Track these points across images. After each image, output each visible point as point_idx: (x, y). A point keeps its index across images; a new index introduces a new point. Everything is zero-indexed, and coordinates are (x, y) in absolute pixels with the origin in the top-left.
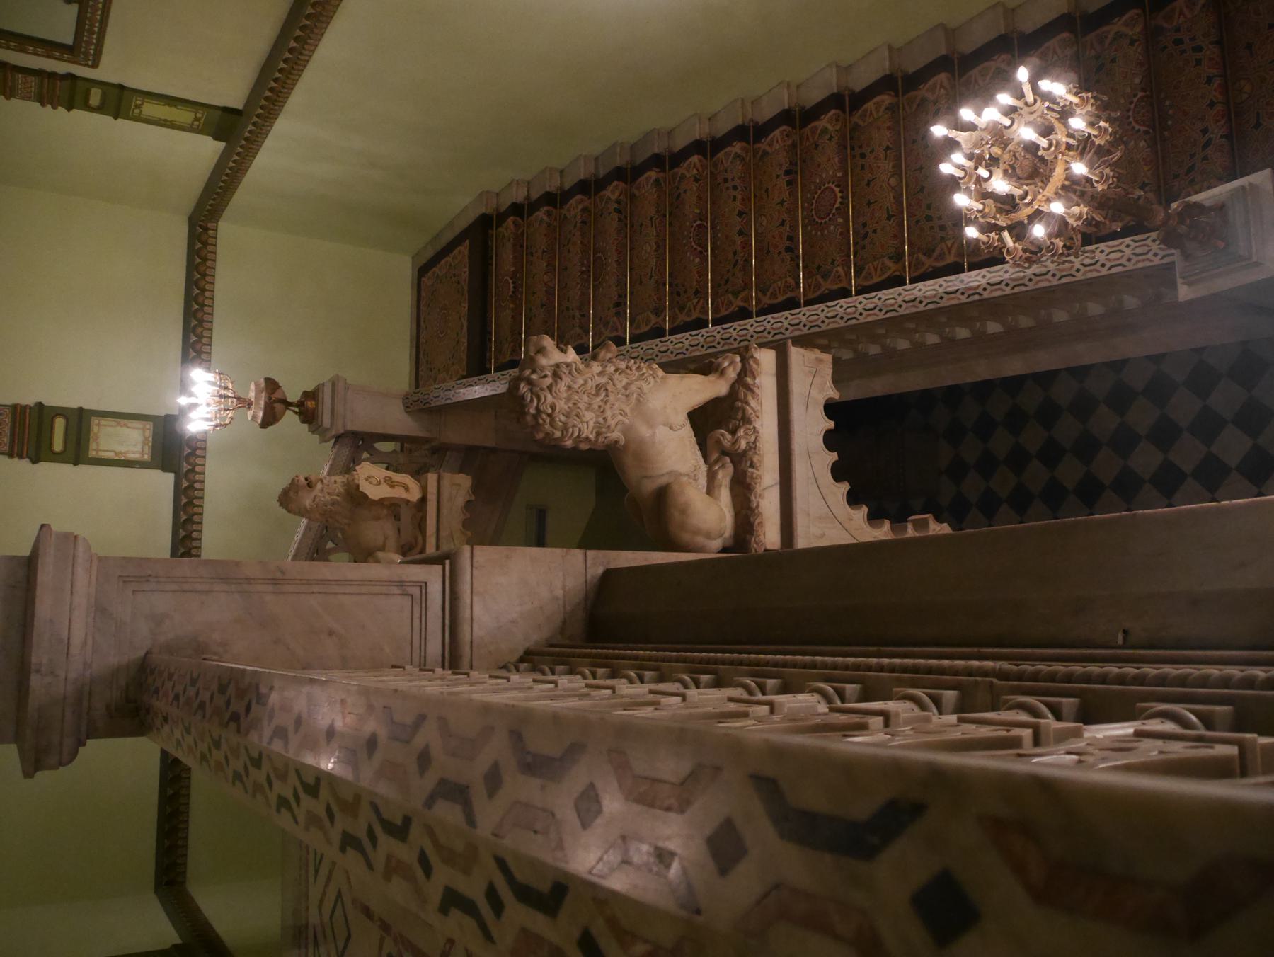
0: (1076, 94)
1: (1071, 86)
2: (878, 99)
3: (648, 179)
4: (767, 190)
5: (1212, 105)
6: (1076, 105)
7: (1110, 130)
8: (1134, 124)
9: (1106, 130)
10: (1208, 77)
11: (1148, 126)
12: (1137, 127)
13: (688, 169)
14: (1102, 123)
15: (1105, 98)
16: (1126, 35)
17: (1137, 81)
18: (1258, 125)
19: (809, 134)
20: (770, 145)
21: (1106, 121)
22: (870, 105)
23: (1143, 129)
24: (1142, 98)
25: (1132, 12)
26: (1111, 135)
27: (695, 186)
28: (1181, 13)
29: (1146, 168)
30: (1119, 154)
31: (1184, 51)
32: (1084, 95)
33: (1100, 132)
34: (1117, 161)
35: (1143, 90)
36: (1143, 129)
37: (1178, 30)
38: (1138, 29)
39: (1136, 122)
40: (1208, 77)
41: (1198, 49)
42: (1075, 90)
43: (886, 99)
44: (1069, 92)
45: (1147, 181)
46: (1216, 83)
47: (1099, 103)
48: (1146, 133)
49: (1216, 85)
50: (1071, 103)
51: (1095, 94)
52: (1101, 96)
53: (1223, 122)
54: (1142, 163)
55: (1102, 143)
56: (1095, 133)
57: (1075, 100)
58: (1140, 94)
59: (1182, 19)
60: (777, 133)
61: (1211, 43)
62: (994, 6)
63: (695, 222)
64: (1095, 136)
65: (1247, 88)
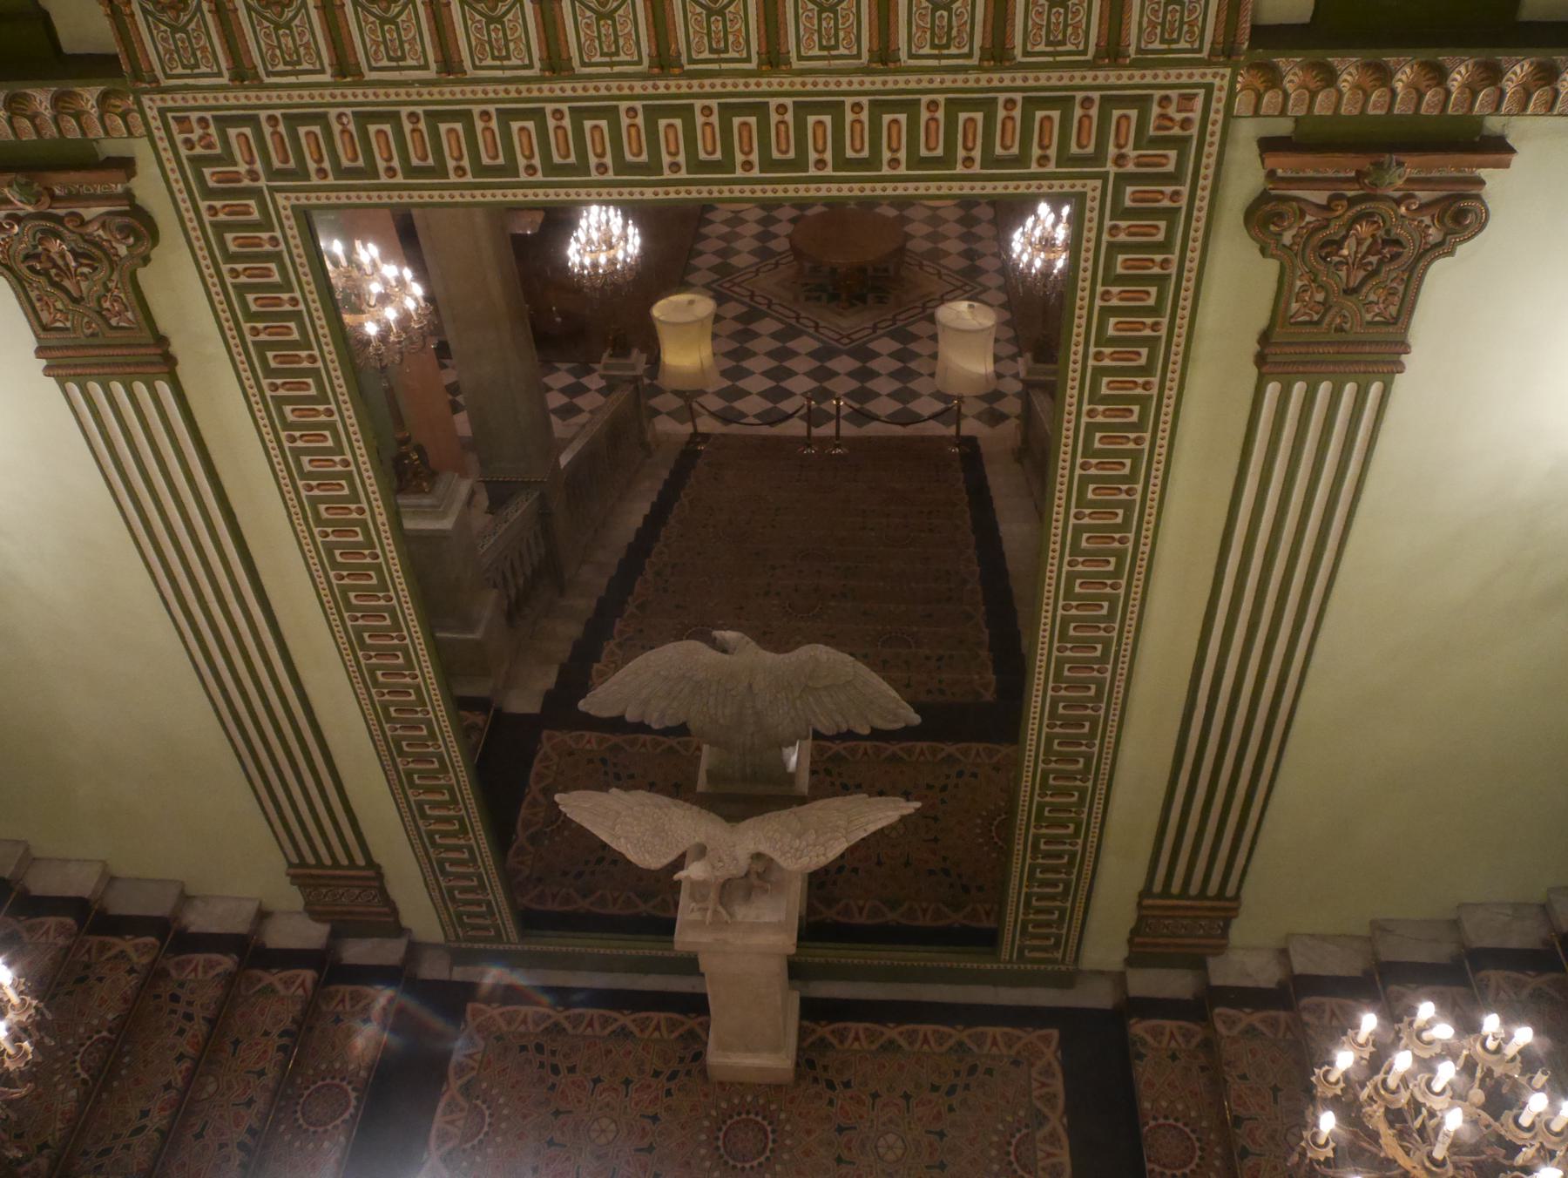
0: (21, 993)
1: (23, 980)
2: (215, 957)
3: (210, 965)
4: (236, 1043)
5: (168, 1087)
6: (13, 1006)
7: (30, 1057)
8: (78, 1065)
9: (26, 1054)
10: (181, 1054)
11: (91, 1076)
12: (79, 1070)
13: (287, 983)
14: (26, 1044)
15: (49, 1016)
16: (129, 960)
17: (110, 1017)
18: (199, 1136)
19: (1054, 1160)
20: (180, 966)
21: (31, 1043)
22: (200, 958)
23: (84, 1075)
24: (103, 1039)
25: (150, 940)
26: (27, 1064)
27: (128, 983)
28: (195, 969)
29: (59, 1125)
30: (24, 1091)
31: (174, 1012)
32: (28, 999)
33: (17, 1054)
34: (17, 1100)
35: (110, 1031)
36: (84, 1075)
37: (181, 985)
38: (145, 960)
39: (82, 1063)
40: (181, 1054)
41: (189, 1017)
42: (23, 988)
43: (227, 963)
44: (15, 986)
45: (50, 1142)
46: (186, 1064)
47: (38, 1018)
48: (84, 1082)
49: (183, 1067)
50: (9, 1001)
51: (41, 1005)
52: (46, 1012)
53: (167, 1113)
54: (59, 1117)
55: (12, 1068)
56: (11, 1051)
57: (15, 999)
58: (105, 1033)
59: (192, 976)
60: (51, 921)
61: (204, 1018)
62: (17, 842)
63: (98, 1032)
64: (9, 1056)
65: (211, 1088)
